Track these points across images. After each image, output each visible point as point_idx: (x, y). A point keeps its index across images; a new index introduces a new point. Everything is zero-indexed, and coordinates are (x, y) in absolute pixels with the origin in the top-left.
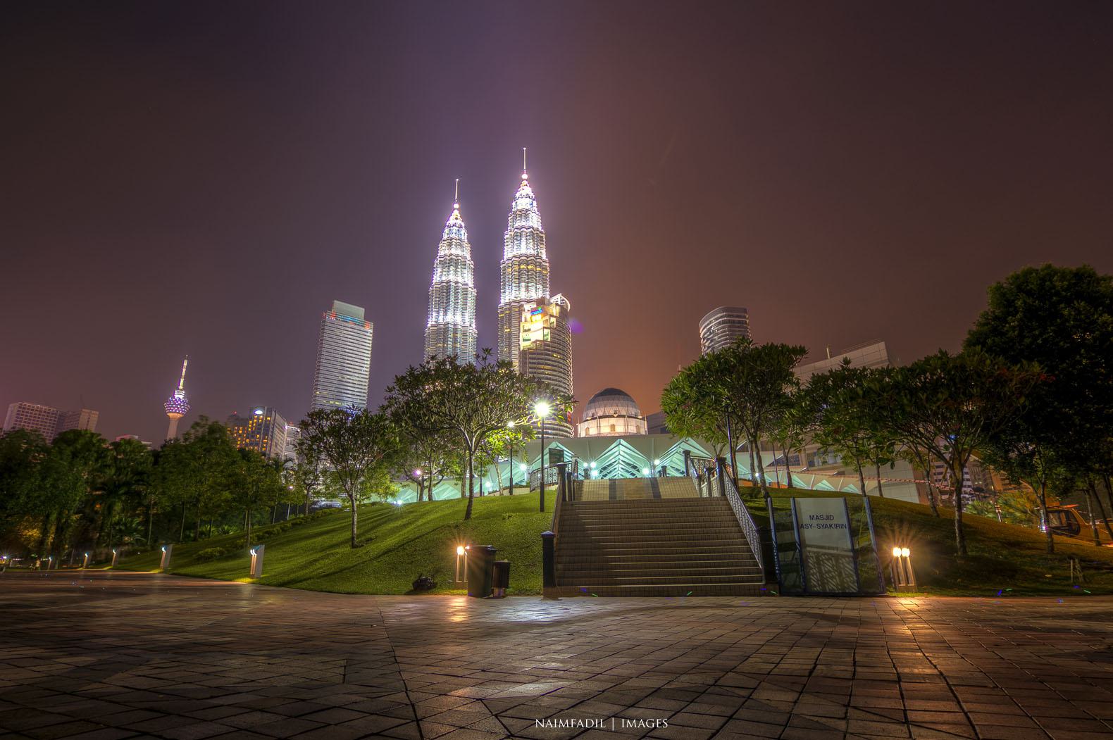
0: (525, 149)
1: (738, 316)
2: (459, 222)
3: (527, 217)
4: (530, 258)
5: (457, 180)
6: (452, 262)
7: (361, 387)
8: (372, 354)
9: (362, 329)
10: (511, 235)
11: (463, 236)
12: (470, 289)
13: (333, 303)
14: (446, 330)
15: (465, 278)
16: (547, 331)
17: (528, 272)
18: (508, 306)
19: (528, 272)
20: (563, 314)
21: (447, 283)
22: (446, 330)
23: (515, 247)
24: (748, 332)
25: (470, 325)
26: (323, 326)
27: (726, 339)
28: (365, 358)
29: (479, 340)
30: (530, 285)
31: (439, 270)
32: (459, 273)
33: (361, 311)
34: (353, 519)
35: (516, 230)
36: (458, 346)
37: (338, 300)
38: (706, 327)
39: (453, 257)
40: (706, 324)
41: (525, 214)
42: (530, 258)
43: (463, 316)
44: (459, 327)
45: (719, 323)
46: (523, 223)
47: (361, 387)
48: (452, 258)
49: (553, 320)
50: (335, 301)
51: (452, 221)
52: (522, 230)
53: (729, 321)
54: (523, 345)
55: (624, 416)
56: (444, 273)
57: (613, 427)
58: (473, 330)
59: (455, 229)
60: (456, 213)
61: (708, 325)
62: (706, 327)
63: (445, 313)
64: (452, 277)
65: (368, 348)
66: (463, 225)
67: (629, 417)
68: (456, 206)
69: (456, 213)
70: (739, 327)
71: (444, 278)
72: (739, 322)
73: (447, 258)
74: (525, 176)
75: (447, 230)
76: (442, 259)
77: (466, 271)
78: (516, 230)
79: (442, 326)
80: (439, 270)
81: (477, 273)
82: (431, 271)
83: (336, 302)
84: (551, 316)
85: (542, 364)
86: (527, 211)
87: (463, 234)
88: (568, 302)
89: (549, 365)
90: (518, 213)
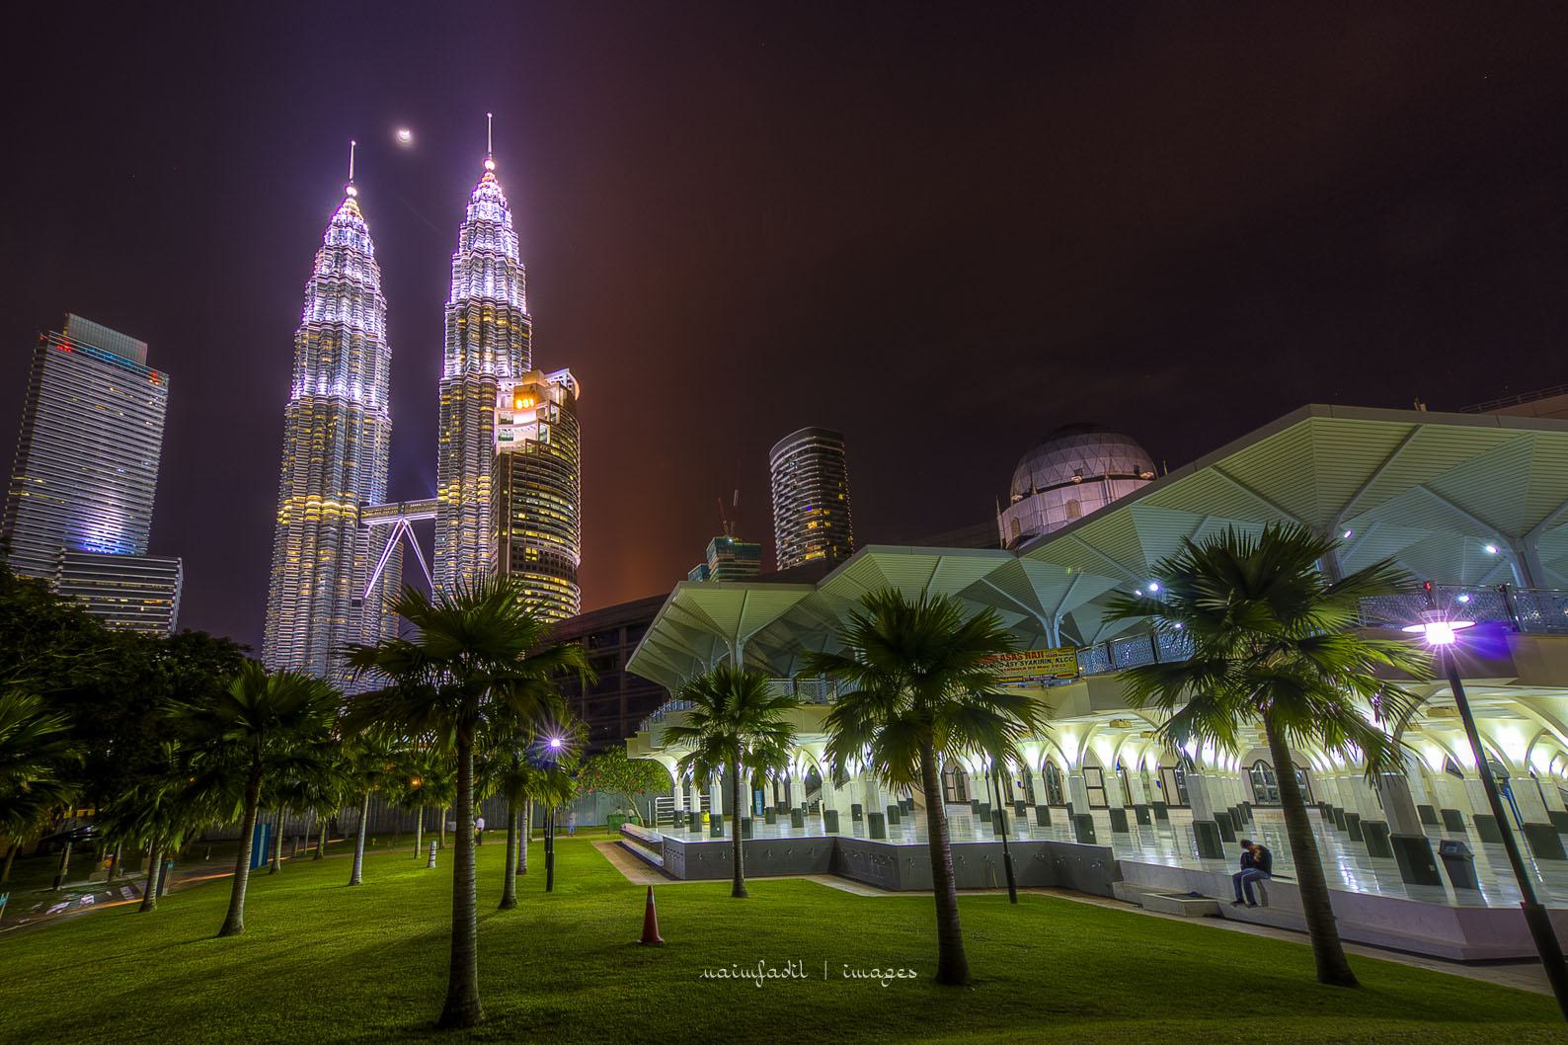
0: (490, 115)
1: (830, 444)
2: (359, 220)
3: (495, 236)
4: (500, 307)
5: (353, 143)
6: (340, 290)
7: (139, 494)
8: (164, 433)
9: (144, 382)
10: (466, 261)
11: (366, 249)
12: (380, 346)
13: (67, 319)
14: (331, 411)
15: (371, 324)
16: (544, 427)
17: (497, 330)
18: (459, 383)
19: (497, 330)
20: (569, 403)
21: (335, 326)
22: (331, 411)
23: (474, 283)
24: (843, 468)
25: (380, 409)
26: (35, 373)
27: (815, 476)
28: (144, 488)
29: (395, 440)
30: (500, 351)
31: (318, 301)
32: (360, 314)
33: (140, 348)
34: (416, 847)
35: (475, 254)
36: (356, 440)
37: (76, 314)
38: (782, 455)
39: (347, 281)
40: (784, 450)
41: (491, 229)
42: (500, 307)
43: (367, 392)
44: (359, 408)
45: (800, 454)
46: (490, 246)
47: (139, 494)
48: (345, 284)
49: (555, 410)
50: (72, 316)
51: (342, 216)
52: (487, 256)
53: (819, 450)
54: (500, 446)
55: (1101, 478)
56: (329, 307)
57: (1073, 505)
58: (383, 420)
59: (350, 233)
60: (351, 204)
61: (787, 452)
62: (782, 455)
63: (331, 380)
64: (345, 317)
65: (154, 448)
66: (365, 227)
67: (1113, 477)
68: (352, 191)
69: (351, 204)
70: (832, 460)
71: (329, 317)
72: (833, 452)
73: (336, 281)
74: (490, 165)
75: (333, 231)
76: (325, 282)
77: (373, 312)
78: (475, 254)
79: (325, 402)
80: (318, 301)
81: (391, 318)
82: (300, 301)
83: (74, 319)
84: (552, 403)
85: (536, 480)
86: (496, 225)
87: (366, 244)
88: (576, 383)
89: (547, 484)
90: (478, 224)
